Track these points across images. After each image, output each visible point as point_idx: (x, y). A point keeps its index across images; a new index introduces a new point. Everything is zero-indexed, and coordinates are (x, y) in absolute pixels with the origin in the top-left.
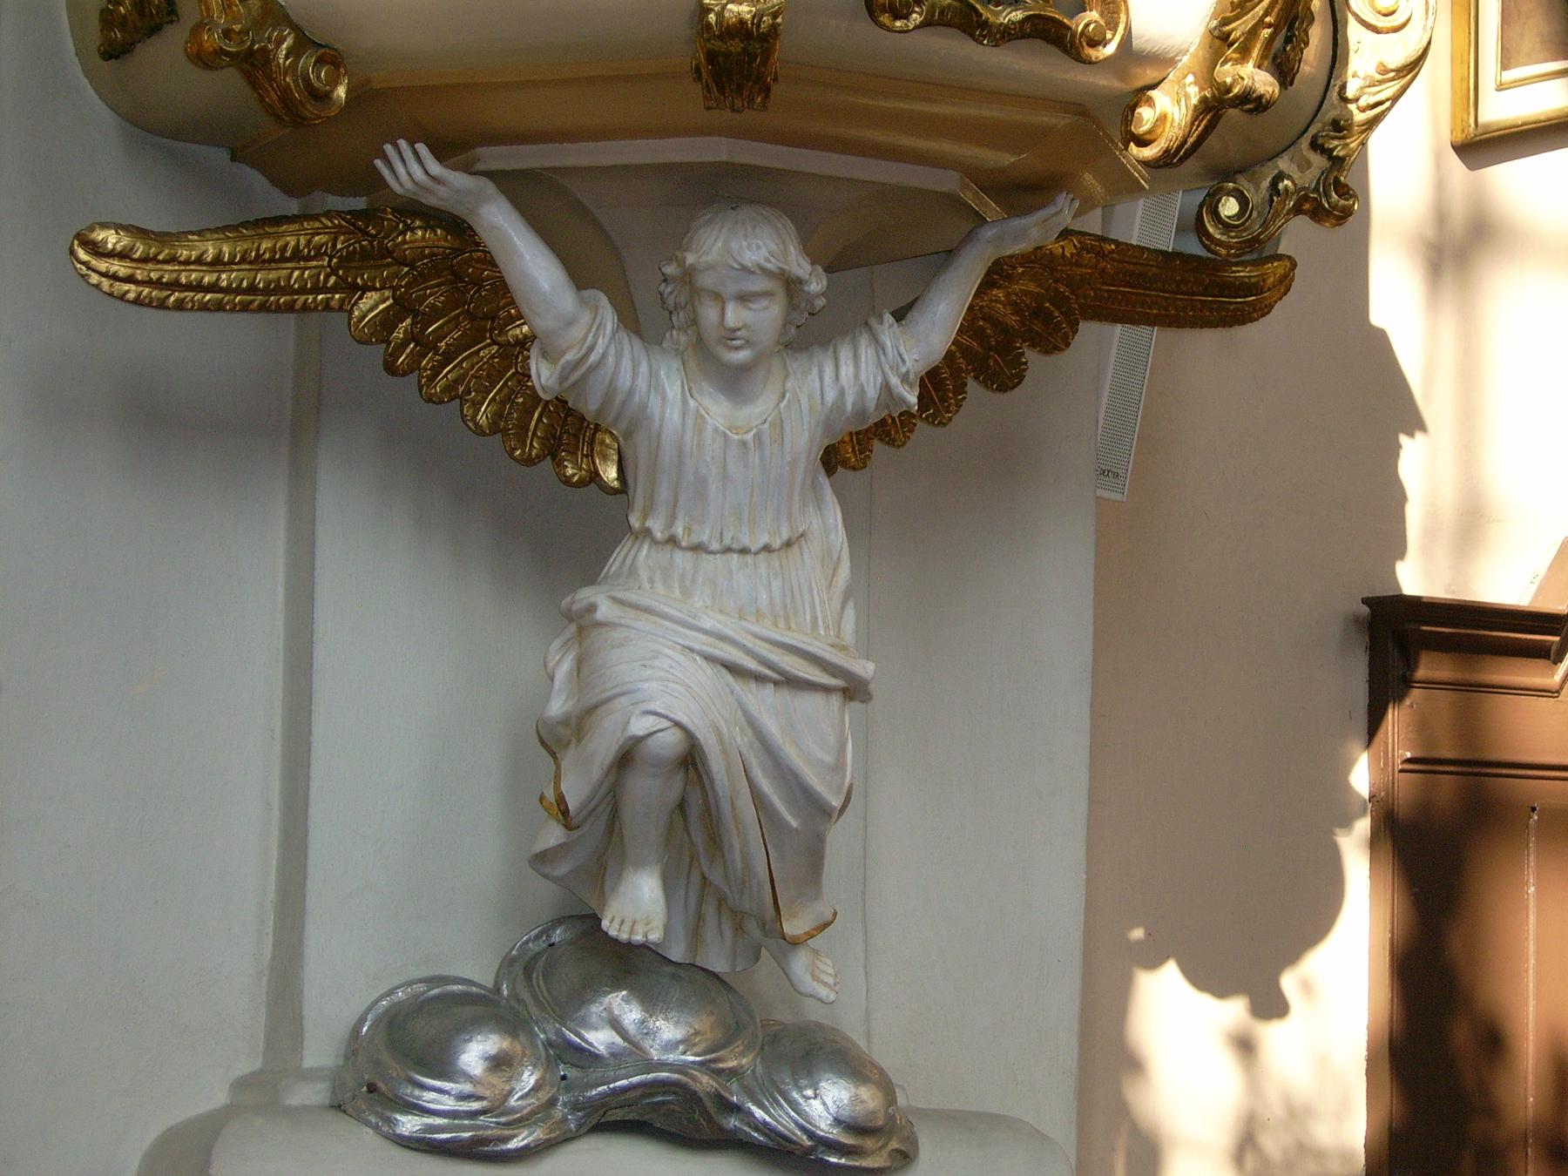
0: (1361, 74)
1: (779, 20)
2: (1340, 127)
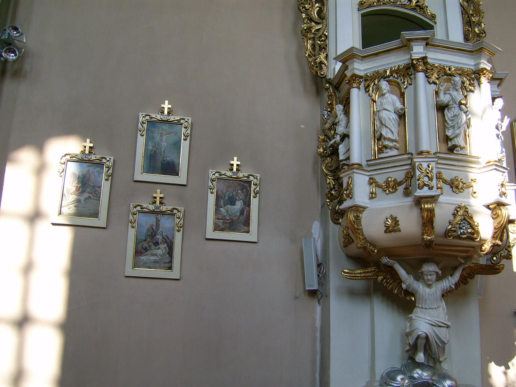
0: (511, 239)
1: (434, 239)
2: (509, 247)
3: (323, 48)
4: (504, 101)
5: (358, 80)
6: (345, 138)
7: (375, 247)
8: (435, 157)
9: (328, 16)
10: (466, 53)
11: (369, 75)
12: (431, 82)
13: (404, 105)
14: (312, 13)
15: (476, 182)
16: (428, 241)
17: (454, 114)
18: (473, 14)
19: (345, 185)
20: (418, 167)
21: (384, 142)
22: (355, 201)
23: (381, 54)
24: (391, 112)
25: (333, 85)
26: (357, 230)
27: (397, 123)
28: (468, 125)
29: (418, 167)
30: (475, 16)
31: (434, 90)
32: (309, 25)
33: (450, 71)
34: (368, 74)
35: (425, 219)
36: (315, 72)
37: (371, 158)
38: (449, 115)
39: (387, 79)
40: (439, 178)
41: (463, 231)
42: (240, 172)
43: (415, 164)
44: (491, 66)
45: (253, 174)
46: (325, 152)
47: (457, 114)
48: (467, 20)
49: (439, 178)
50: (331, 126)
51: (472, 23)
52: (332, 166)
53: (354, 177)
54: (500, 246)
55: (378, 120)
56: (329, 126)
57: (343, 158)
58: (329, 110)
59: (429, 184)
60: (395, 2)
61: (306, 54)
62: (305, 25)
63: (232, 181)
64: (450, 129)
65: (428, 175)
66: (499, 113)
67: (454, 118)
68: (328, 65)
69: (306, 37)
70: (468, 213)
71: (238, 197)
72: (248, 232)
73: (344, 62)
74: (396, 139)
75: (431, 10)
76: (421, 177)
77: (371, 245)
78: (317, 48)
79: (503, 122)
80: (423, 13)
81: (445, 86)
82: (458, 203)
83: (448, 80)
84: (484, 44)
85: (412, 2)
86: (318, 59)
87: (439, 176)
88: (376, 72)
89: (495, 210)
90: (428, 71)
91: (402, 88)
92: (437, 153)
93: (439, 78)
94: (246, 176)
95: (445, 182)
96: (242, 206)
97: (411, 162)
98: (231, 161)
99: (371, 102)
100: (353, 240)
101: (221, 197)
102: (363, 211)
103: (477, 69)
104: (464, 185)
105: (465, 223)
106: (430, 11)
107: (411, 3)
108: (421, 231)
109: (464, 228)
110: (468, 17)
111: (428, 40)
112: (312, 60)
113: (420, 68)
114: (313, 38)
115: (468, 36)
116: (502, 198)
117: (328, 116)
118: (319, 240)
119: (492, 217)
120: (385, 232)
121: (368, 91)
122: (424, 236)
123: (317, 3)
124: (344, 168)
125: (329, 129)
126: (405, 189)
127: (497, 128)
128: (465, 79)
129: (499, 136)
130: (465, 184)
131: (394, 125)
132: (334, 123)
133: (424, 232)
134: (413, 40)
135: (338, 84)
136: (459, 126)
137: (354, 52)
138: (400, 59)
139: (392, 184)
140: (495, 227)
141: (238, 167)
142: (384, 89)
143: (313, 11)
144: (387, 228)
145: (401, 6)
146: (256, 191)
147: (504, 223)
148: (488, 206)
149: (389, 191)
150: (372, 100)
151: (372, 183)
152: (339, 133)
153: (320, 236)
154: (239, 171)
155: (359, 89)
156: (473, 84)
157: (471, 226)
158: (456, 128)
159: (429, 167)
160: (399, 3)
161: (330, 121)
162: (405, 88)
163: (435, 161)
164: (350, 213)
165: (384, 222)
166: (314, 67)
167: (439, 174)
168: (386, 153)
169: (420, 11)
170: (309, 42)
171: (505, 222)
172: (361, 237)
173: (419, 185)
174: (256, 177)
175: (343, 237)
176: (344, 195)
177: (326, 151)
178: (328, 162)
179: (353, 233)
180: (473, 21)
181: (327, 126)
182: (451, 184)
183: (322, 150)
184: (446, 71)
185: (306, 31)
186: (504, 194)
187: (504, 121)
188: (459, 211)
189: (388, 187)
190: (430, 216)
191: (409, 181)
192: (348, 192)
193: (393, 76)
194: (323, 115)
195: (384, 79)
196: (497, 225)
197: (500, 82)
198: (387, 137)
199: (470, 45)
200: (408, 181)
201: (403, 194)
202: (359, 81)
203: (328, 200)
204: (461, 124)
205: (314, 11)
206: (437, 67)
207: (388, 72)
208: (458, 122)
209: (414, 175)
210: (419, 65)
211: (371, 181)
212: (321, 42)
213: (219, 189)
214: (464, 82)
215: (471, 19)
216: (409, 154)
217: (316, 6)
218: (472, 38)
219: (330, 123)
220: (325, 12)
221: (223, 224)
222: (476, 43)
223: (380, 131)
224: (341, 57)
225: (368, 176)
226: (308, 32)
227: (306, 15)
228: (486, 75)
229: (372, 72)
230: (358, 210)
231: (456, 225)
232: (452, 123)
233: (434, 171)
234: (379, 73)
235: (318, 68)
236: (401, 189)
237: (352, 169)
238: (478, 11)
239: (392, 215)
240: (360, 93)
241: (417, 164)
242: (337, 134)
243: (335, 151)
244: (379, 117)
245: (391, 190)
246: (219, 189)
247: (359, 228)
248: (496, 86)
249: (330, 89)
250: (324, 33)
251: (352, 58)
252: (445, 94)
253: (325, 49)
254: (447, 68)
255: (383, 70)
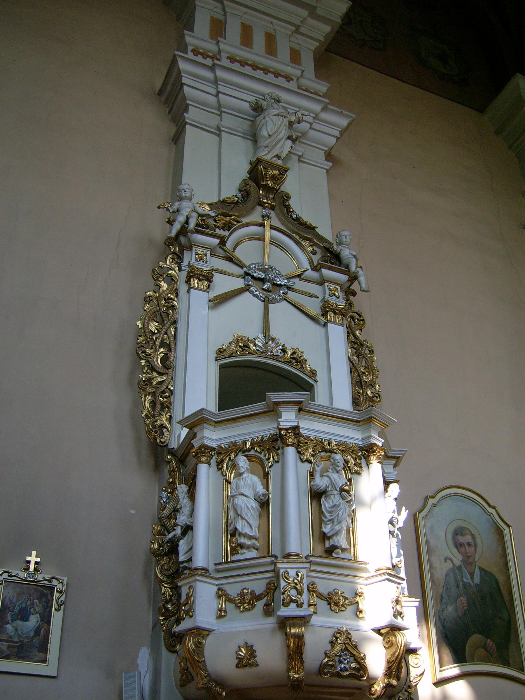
0: (413, 676)
1: (304, 678)
2: (410, 687)
3: (166, 407)
4: (400, 488)
5: (209, 452)
6: (188, 531)
7: (223, 688)
8: (306, 562)
9: (176, 366)
10: (351, 423)
11: (223, 447)
12: (304, 460)
13: (268, 490)
14: (154, 360)
15: (362, 597)
16: (294, 681)
17: (334, 504)
18: (364, 372)
19: (184, 598)
20: (283, 576)
21: (239, 539)
22: (197, 621)
23: (240, 420)
24: (250, 498)
25: (176, 457)
26: (197, 663)
27: (258, 514)
28: (352, 518)
29: (283, 576)
30: (367, 375)
31: (307, 471)
32: (149, 375)
33: (329, 446)
34: (223, 445)
35: (291, 649)
36: (153, 438)
37: (222, 560)
38: (327, 505)
39: (247, 453)
40: (313, 591)
41: (345, 667)
42: (38, 572)
43: (279, 571)
44: (383, 441)
45: (57, 577)
46: (160, 549)
47: (337, 504)
48: (357, 379)
49: (313, 591)
50: (171, 514)
51: (363, 383)
52: (169, 569)
53: (197, 587)
54: (395, 687)
55: (232, 508)
56: (168, 513)
57: (183, 559)
58: (169, 491)
59: (298, 599)
60: (265, 353)
61: (143, 413)
62: (144, 375)
63: (26, 586)
64: (327, 524)
65: (297, 586)
66: (395, 503)
67: (334, 509)
68: (171, 431)
69: (143, 391)
70: (350, 641)
71: (33, 609)
72: (44, 661)
73: (191, 427)
74: (256, 535)
75: (311, 364)
76: (287, 590)
77: (217, 684)
78: (158, 406)
79: (400, 515)
80: (301, 368)
81: (322, 466)
82: (337, 626)
83: (327, 458)
84: (373, 412)
85: (286, 352)
86: (159, 421)
87: (313, 589)
88: (232, 443)
89: (388, 637)
90: (300, 445)
91: (266, 466)
92: (310, 556)
93: (315, 454)
94: (48, 579)
95: (320, 596)
96: (39, 623)
97: (275, 568)
98: (27, 557)
99: (224, 483)
100: (192, 677)
101: (9, 608)
102: (208, 635)
103: (364, 445)
104: (346, 601)
105: (346, 654)
106: (309, 366)
107: (285, 354)
108: (286, 666)
109: (346, 661)
110: (359, 375)
111: (302, 404)
112: (150, 422)
113: (290, 440)
114: (154, 392)
115: (358, 399)
116: (397, 619)
117: (168, 498)
118: (148, 674)
119: (384, 647)
120: (237, 666)
121: (221, 468)
122: (290, 674)
123: (162, 348)
124: (184, 572)
125: (168, 517)
126: (265, 605)
127: (391, 522)
128: (349, 457)
129: (395, 534)
130: (347, 599)
131: (253, 515)
132: (176, 509)
133: (291, 667)
134: (282, 403)
135: (184, 455)
136: (339, 520)
137: (204, 415)
138: (264, 428)
139: (248, 597)
140: (387, 660)
141: (37, 565)
142: (242, 467)
143: (156, 357)
144: (239, 661)
145: (272, 357)
146: (59, 601)
147: (400, 655)
148: (379, 630)
149: (244, 608)
150: (225, 481)
151: (222, 596)
152: (180, 524)
153: (149, 670)
154: (37, 572)
155: (209, 465)
156: (360, 464)
157: (354, 659)
158: (336, 523)
159: (298, 575)
160: (269, 353)
161: (170, 506)
162: (270, 467)
163: (307, 568)
164: (188, 638)
165: (236, 652)
166: (152, 431)
167: (312, 585)
168: (242, 554)
169: (296, 365)
170: (148, 397)
171: (401, 653)
172: (202, 673)
173: (283, 600)
174: (61, 581)
175: (179, 673)
176: (182, 612)
177: (163, 547)
178: (164, 564)
179: (192, 667)
180: (365, 381)
181: (166, 512)
182: (329, 600)
183: (157, 546)
184: (325, 446)
185: (145, 382)
186: (400, 614)
187: (401, 513)
188: (338, 638)
189: (242, 602)
190: (298, 644)
191: (272, 594)
192: (187, 607)
193: (254, 449)
194: (160, 498)
195: (243, 453)
196: (390, 658)
197: (397, 462)
198: (243, 532)
199: (356, 413)
200: (270, 595)
201: (263, 613)
202: (209, 454)
203: (161, 618)
204: (342, 518)
205: (157, 357)
206: (313, 440)
207: (248, 444)
208: (338, 514)
209: (278, 586)
210: (288, 437)
211: (220, 593)
212: (163, 399)
213: (6, 597)
214: (348, 461)
215: (362, 378)
216: (272, 556)
217: (160, 351)
218: (363, 403)
219: (170, 509)
220: (171, 360)
221: (7, 649)
222: (369, 409)
223: (234, 524)
224: (187, 421)
225: (216, 585)
226: (148, 384)
227: (146, 362)
228: (376, 453)
229: (228, 443)
230: (200, 634)
231: (334, 658)
232: (331, 516)
233: (305, 581)
234: (236, 444)
235: (158, 434)
236: (260, 605)
237: (194, 575)
238: (371, 368)
239: (246, 642)
240: (211, 470)
241: (282, 571)
242: (177, 525)
243: (174, 549)
244: (233, 505)
245: (246, 606)
246: (6, 597)
247: (200, 660)
248: (392, 466)
249: (172, 462)
250: (168, 388)
251: (201, 423)
252: (322, 476)
253: (168, 408)
254: (326, 442)
255: (241, 441)
